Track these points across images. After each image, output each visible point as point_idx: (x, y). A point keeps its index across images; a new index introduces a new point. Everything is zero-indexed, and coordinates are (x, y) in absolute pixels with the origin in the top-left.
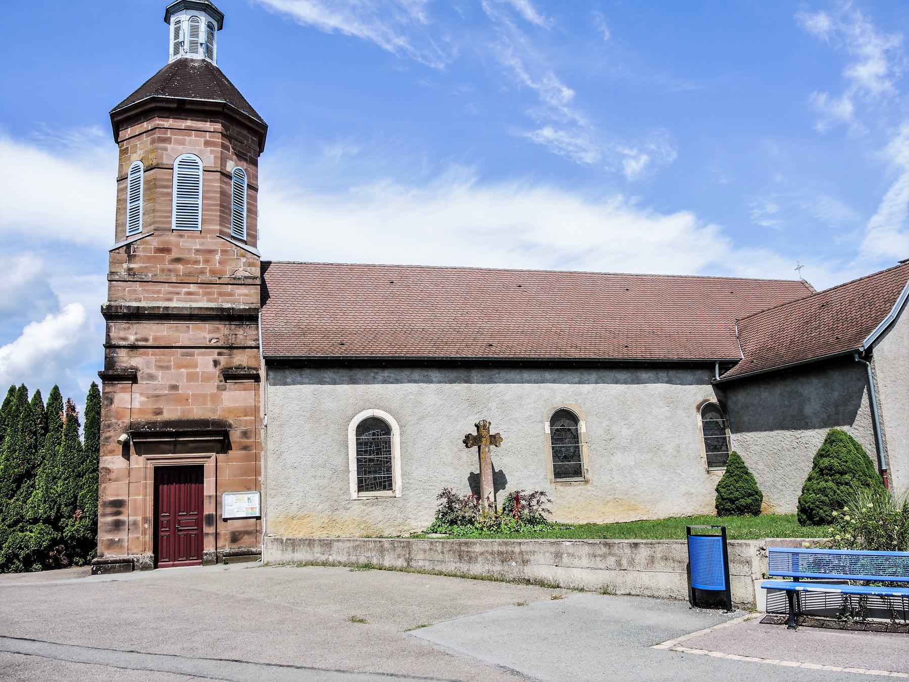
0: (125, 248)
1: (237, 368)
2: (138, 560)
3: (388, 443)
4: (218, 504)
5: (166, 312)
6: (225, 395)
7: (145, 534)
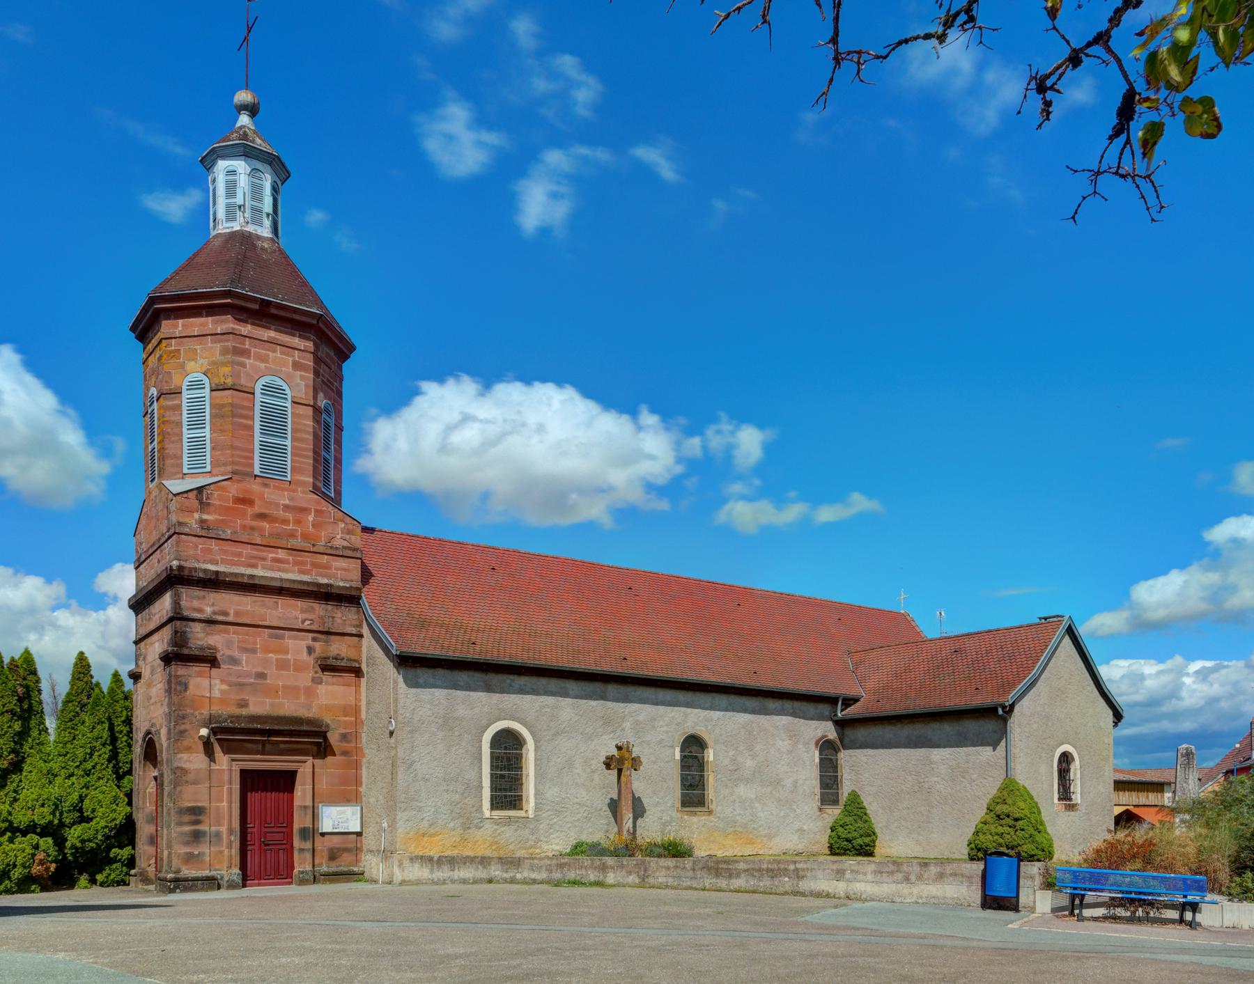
3: (519, 758)
4: (315, 816)
5: (251, 582)
6: (322, 689)
7: (231, 848)
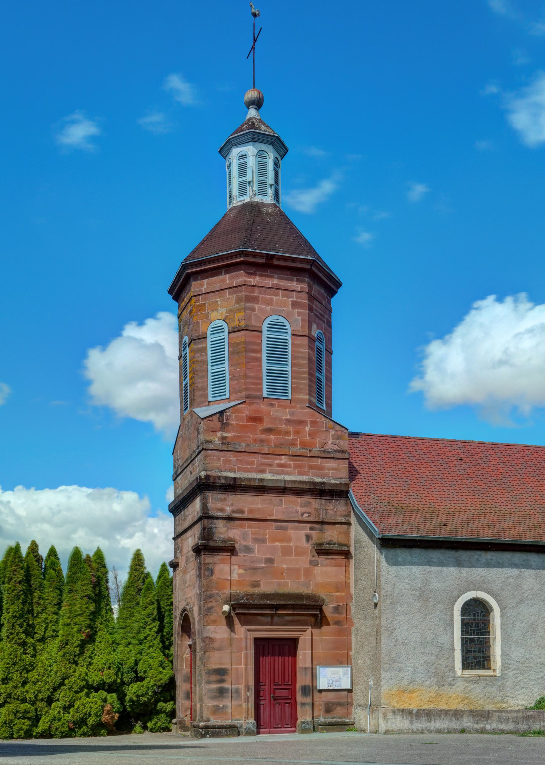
0: (218, 415)
1: (329, 544)
2: (241, 726)
3: (487, 623)
4: (313, 676)
5: (261, 484)
6: (318, 570)
7: (248, 702)
